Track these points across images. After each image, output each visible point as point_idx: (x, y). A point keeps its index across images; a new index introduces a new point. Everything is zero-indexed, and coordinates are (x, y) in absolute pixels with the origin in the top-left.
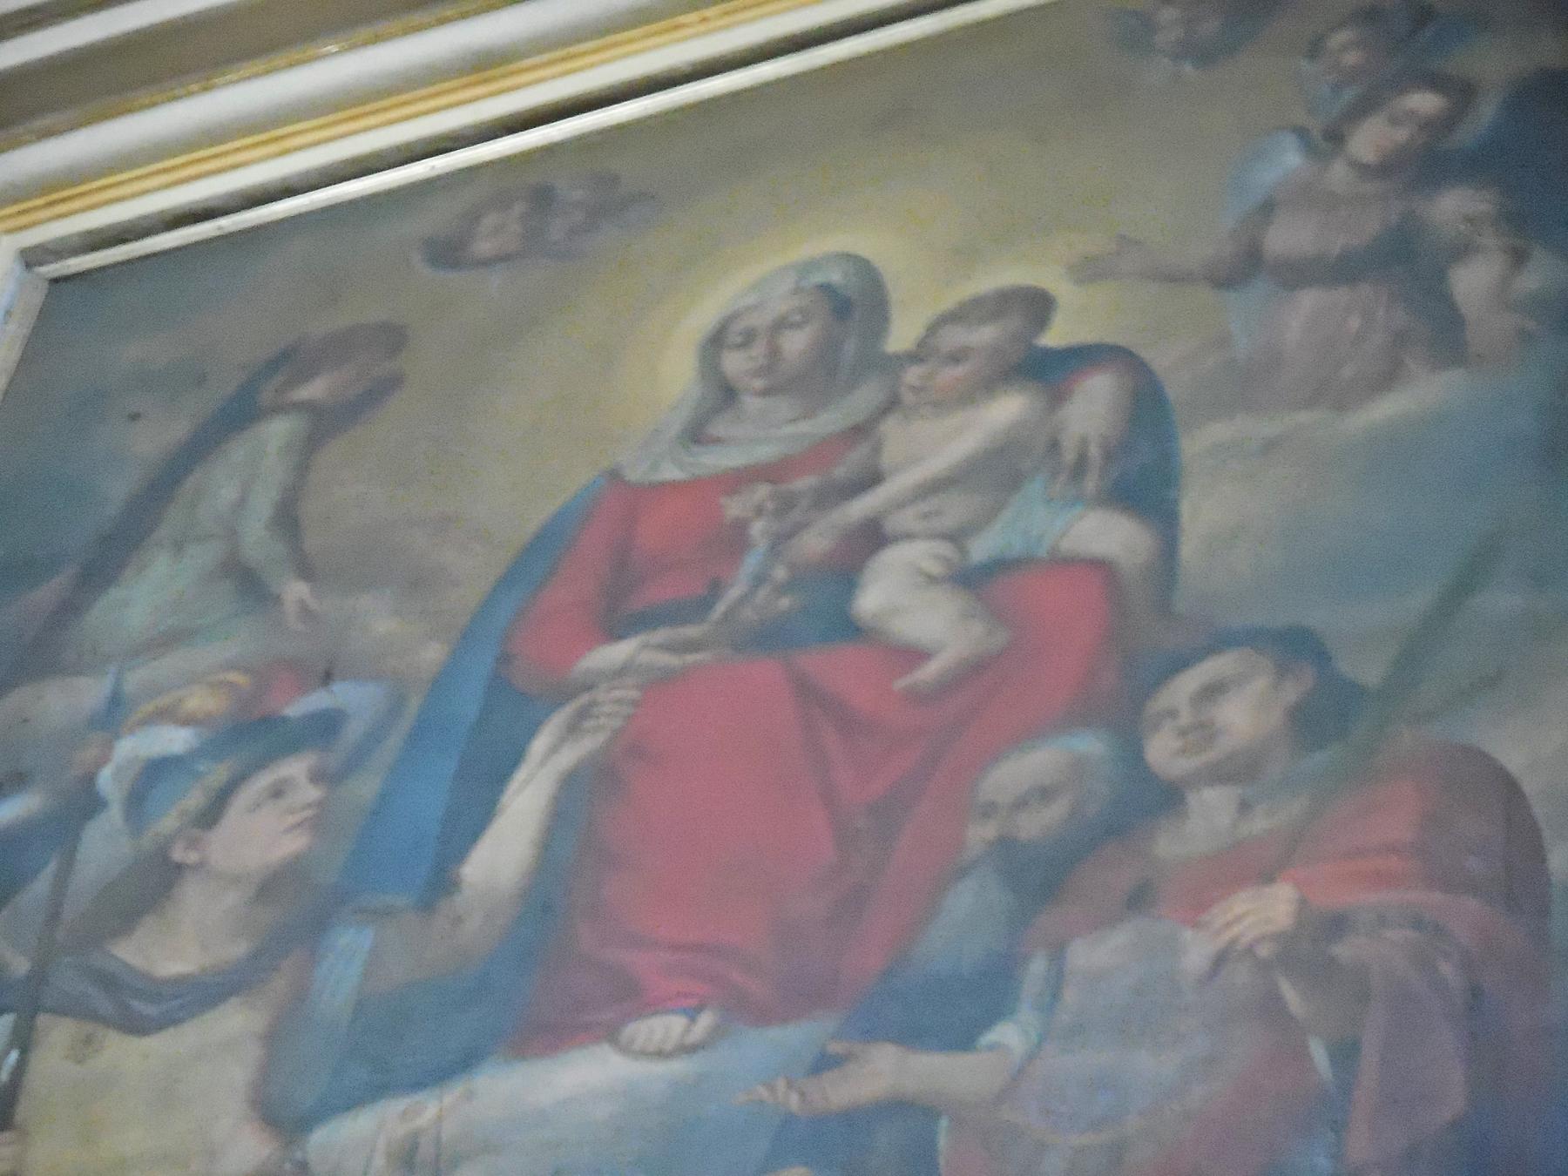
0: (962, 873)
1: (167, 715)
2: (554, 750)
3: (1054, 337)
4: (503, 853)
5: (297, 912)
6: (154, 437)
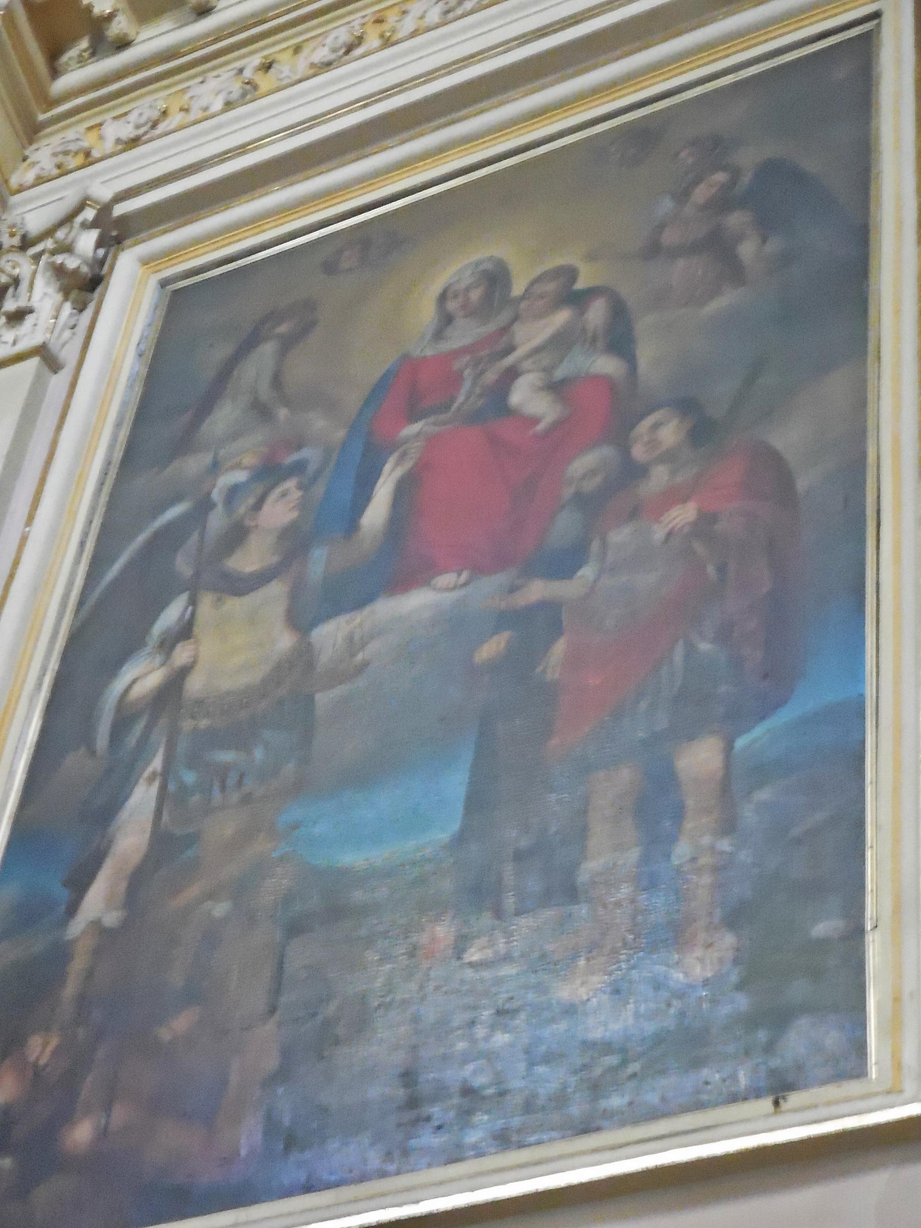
0: (563, 507)
1: (238, 466)
2: (393, 470)
3: (580, 285)
4: (377, 512)
5: (295, 543)
6: (222, 351)
